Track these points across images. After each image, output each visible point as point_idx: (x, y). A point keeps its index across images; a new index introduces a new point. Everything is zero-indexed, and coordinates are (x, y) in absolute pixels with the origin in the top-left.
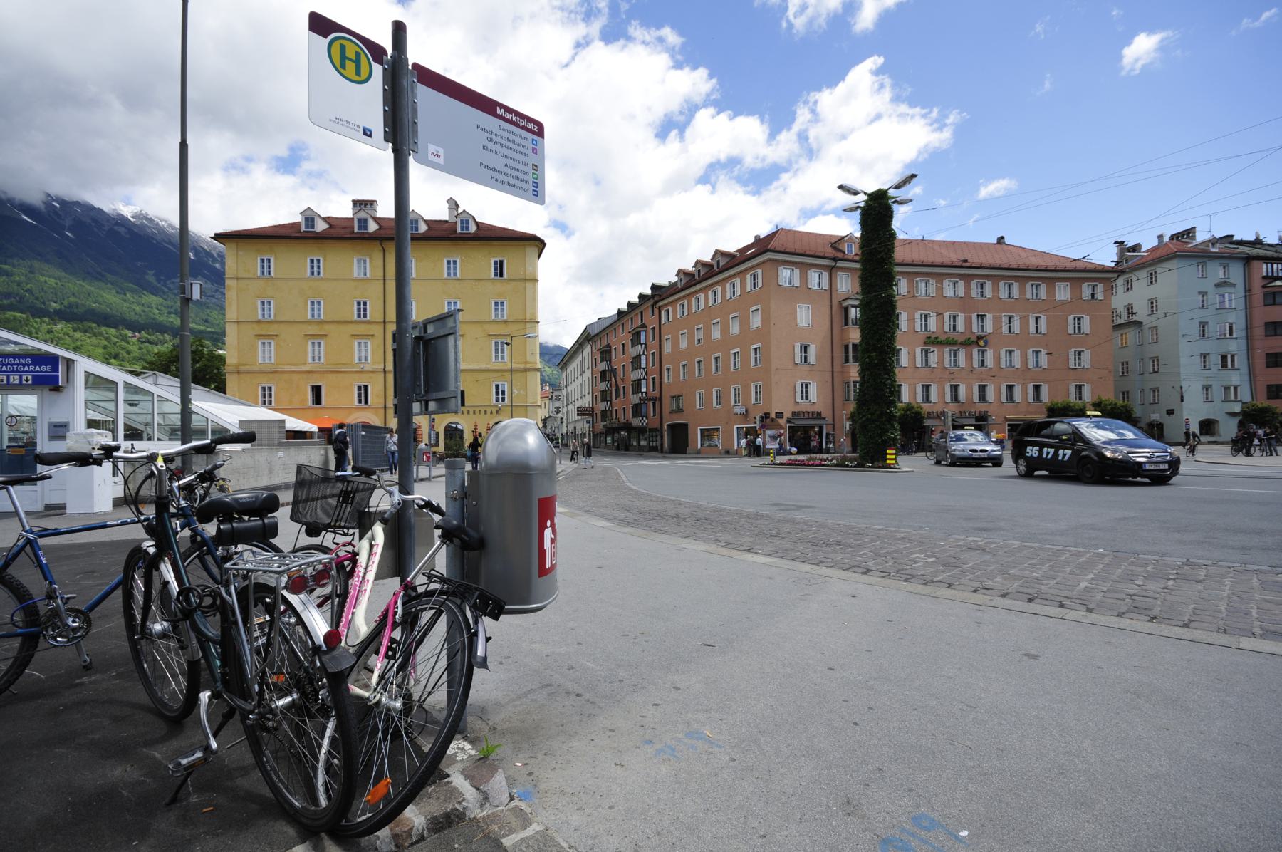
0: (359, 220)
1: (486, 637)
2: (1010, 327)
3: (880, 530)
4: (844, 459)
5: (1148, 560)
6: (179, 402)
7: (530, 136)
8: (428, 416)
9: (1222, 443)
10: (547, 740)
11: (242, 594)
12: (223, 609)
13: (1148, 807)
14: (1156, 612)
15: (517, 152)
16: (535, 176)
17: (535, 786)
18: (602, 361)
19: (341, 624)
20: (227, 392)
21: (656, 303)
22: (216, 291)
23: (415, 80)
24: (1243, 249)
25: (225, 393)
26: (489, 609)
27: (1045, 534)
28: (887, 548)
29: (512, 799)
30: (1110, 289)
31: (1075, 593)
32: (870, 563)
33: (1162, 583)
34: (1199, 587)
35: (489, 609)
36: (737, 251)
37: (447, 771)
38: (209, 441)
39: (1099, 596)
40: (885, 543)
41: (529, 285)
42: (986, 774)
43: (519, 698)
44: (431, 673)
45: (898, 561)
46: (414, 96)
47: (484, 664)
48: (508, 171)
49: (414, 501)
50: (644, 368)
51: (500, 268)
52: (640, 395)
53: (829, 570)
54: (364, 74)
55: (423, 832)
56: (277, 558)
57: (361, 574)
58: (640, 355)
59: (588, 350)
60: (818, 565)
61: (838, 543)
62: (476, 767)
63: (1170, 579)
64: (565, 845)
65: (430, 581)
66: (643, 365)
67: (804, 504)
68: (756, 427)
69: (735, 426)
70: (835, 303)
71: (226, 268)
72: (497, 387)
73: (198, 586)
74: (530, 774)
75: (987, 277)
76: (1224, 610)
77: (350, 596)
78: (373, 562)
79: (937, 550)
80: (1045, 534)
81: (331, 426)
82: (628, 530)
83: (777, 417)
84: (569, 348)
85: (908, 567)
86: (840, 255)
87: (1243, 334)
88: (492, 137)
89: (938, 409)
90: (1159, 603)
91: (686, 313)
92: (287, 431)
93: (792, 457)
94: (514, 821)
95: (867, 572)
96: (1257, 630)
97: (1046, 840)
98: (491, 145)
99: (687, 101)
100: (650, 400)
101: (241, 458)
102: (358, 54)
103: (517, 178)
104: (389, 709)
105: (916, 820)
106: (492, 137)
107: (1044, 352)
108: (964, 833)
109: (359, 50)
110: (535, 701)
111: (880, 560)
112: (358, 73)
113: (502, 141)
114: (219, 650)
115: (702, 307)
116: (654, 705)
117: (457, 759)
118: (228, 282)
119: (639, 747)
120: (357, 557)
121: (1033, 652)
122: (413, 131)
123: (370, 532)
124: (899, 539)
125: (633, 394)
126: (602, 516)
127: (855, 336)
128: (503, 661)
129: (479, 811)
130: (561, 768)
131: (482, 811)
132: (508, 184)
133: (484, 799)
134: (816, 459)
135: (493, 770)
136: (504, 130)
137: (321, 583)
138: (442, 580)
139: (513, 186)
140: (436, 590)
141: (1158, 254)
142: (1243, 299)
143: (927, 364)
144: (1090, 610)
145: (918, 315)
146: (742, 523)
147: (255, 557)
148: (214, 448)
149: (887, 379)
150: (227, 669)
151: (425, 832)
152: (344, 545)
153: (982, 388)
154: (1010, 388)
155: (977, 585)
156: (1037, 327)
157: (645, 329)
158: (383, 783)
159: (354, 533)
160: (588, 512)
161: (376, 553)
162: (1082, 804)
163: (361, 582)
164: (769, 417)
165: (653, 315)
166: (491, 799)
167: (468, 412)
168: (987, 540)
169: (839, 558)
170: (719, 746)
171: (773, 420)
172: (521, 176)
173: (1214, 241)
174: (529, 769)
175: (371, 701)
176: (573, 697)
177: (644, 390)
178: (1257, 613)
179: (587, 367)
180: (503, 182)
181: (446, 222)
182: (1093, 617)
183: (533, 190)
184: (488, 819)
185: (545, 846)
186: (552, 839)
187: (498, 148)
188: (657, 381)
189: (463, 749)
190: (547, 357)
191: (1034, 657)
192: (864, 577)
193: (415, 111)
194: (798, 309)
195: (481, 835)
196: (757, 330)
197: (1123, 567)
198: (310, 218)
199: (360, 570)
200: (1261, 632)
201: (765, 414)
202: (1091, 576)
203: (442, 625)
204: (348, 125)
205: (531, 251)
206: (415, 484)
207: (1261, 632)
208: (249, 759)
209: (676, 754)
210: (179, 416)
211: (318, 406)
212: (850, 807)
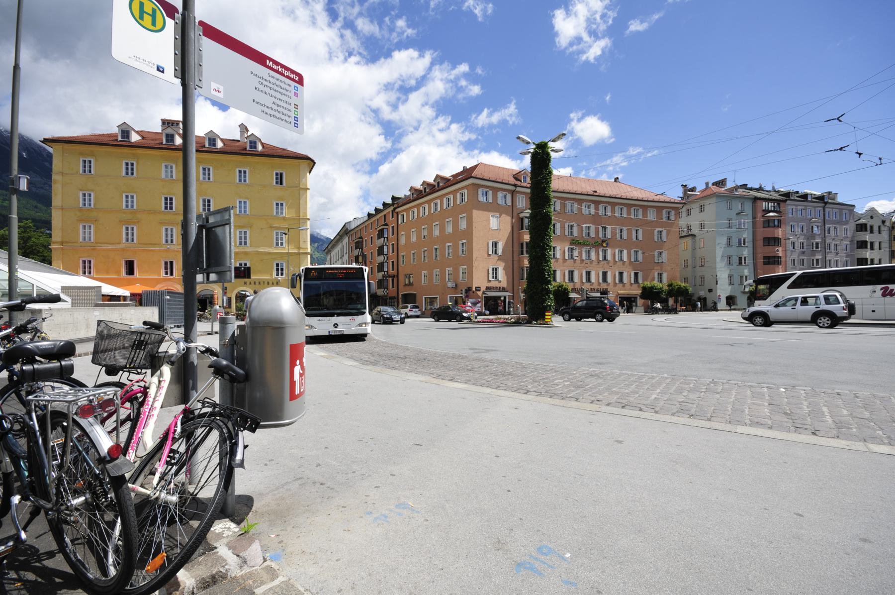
0: (167, 135)
1: (244, 445)
2: (621, 235)
3: (537, 365)
4: (519, 319)
5: (691, 380)
6: (8, 271)
7: (293, 84)
8: (221, 284)
9: (739, 310)
10: (296, 517)
11: (42, 420)
12: (27, 431)
13: (676, 531)
14: (693, 412)
15: (282, 94)
16: (296, 113)
17: (284, 550)
18: (356, 248)
19: (132, 441)
20: (52, 264)
21: (395, 209)
22: (45, 184)
23: (201, 34)
24: (752, 193)
25: (50, 264)
26: (248, 424)
27: (635, 365)
28: (541, 376)
29: (265, 560)
30: (678, 214)
31: (649, 402)
32: (529, 387)
33: (698, 394)
34: (718, 396)
35: (248, 424)
36: (451, 176)
37: (215, 545)
38: (20, 301)
39: (661, 403)
40: (540, 373)
41: (302, 192)
42: (585, 517)
43: (277, 488)
44: (204, 471)
45: (547, 385)
46: (200, 45)
47: (241, 465)
48: (275, 107)
49: (197, 348)
50: (386, 255)
51: (280, 179)
52: (383, 273)
53: (503, 391)
54: (159, 24)
55: (193, 590)
56: (72, 391)
57: (150, 403)
58: (383, 246)
59: (346, 240)
60: (496, 389)
61: (511, 374)
62: (238, 540)
63: (702, 392)
64: (302, 589)
65: (203, 407)
66: (385, 252)
67: (490, 348)
68: (462, 297)
69: (449, 296)
70: (515, 215)
71: (53, 166)
72: (277, 265)
73: (9, 415)
74: (281, 542)
75: (608, 203)
76: (730, 409)
77: (140, 420)
78: (160, 394)
79: (571, 377)
80: (635, 365)
81: (141, 292)
82: (370, 367)
83: (476, 290)
84: (332, 239)
85: (552, 389)
86: (518, 183)
87: (751, 244)
88: (262, 81)
89: (578, 286)
90: (695, 406)
91: (416, 217)
92: (103, 295)
93: (486, 317)
94: (265, 576)
95: (527, 392)
96: (748, 422)
97: (616, 555)
98: (261, 87)
99: (367, 64)
100: (390, 276)
101: (61, 315)
102: (154, 11)
103: (282, 113)
104: (166, 502)
105: (540, 550)
106: (262, 81)
107: (640, 252)
108: (568, 555)
109: (156, 8)
110: (289, 490)
111: (536, 384)
112: (154, 24)
113: (271, 85)
114: (27, 464)
115: (427, 213)
116: (375, 487)
117: (224, 535)
118: (54, 177)
119: (362, 517)
120: (148, 390)
121: (620, 439)
122: (198, 72)
123: (159, 371)
124: (548, 371)
125: (378, 272)
126: (352, 358)
127: (527, 238)
128: (268, 463)
129: (239, 571)
130: (304, 536)
131: (242, 571)
132: (275, 117)
133: (242, 562)
134: (500, 318)
135: (251, 541)
136: (272, 77)
137: (107, 409)
138: (214, 405)
139: (279, 118)
140: (207, 413)
141: (705, 194)
142: (752, 223)
143: (572, 258)
144: (656, 412)
145: (566, 225)
146: (448, 362)
147: (53, 390)
148: (25, 306)
149: (547, 266)
150: (33, 478)
151: (195, 590)
152: (137, 382)
153: (571, 273)
154: (621, 274)
155: (593, 398)
156: (637, 236)
157: (387, 227)
158: (160, 556)
159: (146, 373)
160: (342, 355)
161: (163, 387)
162: (639, 531)
163: (150, 409)
164: (471, 290)
165: (393, 217)
166: (248, 563)
167: (255, 283)
168: (601, 370)
169: (510, 384)
170: (418, 512)
171: (473, 292)
172: (285, 112)
173: (736, 188)
174: (280, 538)
175: (151, 497)
176: (318, 485)
177: (386, 269)
178: (748, 412)
179: (345, 252)
180: (271, 116)
181: (238, 141)
182: (657, 417)
183: (295, 123)
184: (244, 578)
185: (287, 591)
186: (293, 586)
187: (267, 90)
188: (395, 263)
189: (229, 528)
190: (316, 245)
191: (621, 442)
192: (525, 395)
193: (200, 57)
194: (491, 218)
195: (239, 588)
196: (464, 231)
197: (677, 385)
198: (125, 132)
199: (150, 400)
200: (750, 423)
201: (469, 288)
202: (658, 391)
203: (215, 435)
204: (144, 62)
205: (304, 164)
206: (198, 338)
207: (750, 423)
208: (54, 546)
209: (388, 519)
210: (7, 282)
211: (131, 277)
212: (500, 545)
